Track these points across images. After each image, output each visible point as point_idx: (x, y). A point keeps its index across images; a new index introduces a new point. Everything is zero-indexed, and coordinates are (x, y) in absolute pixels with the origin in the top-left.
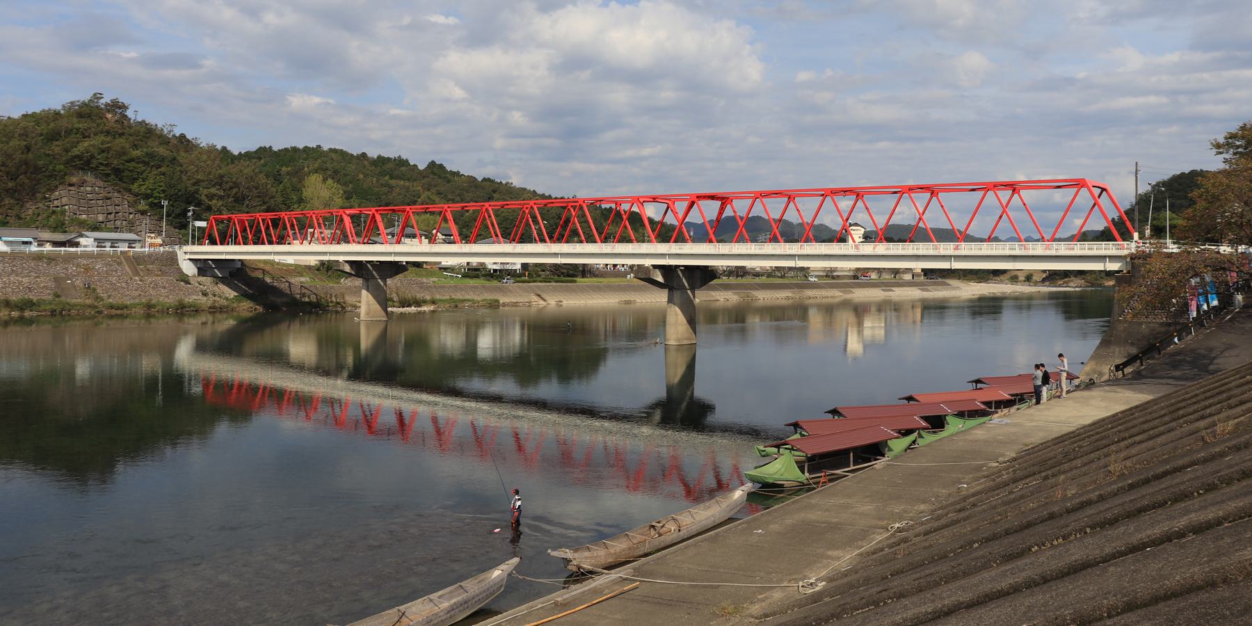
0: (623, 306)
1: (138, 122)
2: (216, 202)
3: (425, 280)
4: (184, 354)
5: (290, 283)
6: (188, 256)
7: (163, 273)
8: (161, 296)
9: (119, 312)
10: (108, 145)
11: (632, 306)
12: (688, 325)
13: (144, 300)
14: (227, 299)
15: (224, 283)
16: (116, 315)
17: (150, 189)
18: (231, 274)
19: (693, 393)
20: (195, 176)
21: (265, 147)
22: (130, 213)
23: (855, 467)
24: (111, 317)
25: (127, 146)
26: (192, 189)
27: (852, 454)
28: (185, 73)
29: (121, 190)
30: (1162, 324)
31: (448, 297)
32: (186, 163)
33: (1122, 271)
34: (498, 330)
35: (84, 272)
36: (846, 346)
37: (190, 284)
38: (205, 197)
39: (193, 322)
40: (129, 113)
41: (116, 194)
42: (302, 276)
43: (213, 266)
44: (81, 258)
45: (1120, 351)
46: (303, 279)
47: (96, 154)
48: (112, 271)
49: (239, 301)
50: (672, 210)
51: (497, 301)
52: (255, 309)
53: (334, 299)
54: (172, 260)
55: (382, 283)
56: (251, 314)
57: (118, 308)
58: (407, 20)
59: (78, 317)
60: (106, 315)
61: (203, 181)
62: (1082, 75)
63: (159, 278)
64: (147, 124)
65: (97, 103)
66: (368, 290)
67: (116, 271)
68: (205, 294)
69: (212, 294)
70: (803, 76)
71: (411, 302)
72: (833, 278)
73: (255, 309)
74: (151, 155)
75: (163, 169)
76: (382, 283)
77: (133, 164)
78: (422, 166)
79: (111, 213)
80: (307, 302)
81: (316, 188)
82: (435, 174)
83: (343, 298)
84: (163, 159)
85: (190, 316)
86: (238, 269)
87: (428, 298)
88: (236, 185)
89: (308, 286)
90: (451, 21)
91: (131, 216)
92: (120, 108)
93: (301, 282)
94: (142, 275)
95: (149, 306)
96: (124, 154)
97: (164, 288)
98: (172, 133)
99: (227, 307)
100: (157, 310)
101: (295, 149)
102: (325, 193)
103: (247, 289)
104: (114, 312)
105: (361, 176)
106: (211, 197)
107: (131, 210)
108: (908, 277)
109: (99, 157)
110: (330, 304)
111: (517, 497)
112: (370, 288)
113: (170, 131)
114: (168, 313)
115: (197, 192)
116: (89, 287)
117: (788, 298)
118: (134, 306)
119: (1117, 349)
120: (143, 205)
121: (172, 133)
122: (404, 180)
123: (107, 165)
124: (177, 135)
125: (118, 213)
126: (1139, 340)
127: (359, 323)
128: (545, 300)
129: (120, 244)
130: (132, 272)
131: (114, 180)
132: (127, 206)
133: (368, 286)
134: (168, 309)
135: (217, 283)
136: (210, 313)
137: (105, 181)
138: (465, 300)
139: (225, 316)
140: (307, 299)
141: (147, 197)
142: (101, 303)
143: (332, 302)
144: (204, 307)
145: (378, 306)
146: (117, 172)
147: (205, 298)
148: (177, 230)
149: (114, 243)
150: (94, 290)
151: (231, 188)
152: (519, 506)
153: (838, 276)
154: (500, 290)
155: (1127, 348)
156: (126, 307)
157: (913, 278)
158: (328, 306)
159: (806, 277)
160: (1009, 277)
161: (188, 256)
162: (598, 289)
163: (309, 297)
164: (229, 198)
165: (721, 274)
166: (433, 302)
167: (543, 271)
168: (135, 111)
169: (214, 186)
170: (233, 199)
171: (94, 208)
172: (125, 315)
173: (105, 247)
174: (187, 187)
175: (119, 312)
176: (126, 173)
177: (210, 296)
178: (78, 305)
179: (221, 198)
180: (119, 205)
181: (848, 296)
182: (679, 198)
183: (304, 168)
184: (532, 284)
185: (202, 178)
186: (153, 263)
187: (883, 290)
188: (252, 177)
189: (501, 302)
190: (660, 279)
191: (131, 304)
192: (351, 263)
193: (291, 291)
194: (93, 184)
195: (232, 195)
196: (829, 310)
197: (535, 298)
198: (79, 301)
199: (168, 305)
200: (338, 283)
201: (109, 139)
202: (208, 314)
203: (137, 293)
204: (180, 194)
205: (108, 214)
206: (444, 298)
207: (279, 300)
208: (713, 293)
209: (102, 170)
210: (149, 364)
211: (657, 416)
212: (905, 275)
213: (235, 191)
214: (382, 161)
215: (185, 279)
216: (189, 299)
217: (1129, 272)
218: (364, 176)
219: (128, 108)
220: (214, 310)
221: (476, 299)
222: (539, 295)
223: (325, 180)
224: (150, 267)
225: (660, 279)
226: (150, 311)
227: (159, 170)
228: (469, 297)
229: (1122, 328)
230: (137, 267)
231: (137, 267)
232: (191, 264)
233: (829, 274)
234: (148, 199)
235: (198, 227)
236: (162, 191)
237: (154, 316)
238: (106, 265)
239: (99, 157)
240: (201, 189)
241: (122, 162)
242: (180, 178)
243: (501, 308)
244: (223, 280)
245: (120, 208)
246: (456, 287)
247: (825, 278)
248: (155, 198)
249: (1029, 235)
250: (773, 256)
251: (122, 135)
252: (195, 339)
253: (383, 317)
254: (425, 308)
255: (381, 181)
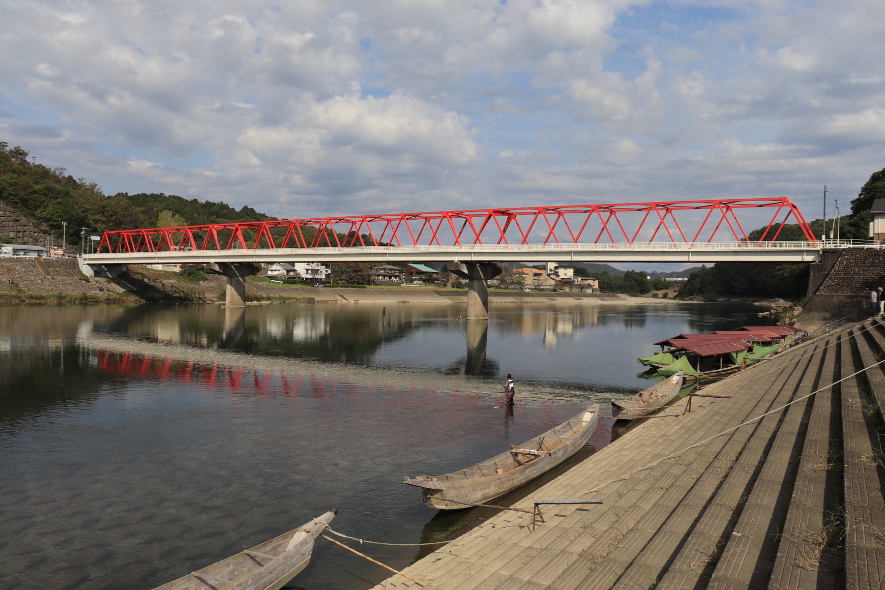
0: (401, 304)
1: (36, 165)
2: (101, 225)
3: (260, 283)
4: (85, 337)
5: (162, 284)
6: (86, 262)
7: (69, 274)
8: (69, 290)
9: (37, 302)
10: (16, 180)
11: (407, 304)
12: (483, 306)
13: (56, 293)
14: (118, 293)
15: (114, 282)
16: (35, 303)
17: (50, 214)
18: (119, 276)
19: (485, 357)
20: (84, 206)
21: (122, 193)
22: (35, 232)
23: (724, 369)
24: (32, 305)
25: (31, 181)
26: (82, 215)
27: (721, 359)
28: (49, 141)
29: (27, 215)
30: (848, 297)
31: (278, 296)
32: (76, 196)
33: (815, 261)
34: (309, 320)
35: (7, 271)
36: (545, 337)
37: (89, 282)
38: (92, 221)
39: (94, 311)
40: (29, 159)
41: (23, 217)
42: (170, 279)
43: (106, 270)
44: (4, 261)
45: (818, 316)
46: (172, 281)
47: (6, 187)
48: (29, 271)
49: (128, 296)
50: (470, 223)
51: (313, 299)
52: (140, 301)
53: (197, 295)
54: (75, 265)
55: (241, 280)
56: (136, 305)
57: (36, 299)
58: (217, 105)
59: (6, 305)
60: (28, 304)
61: (90, 210)
62: (700, 158)
63: (66, 277)
64: (43, 167)
65: (3, 149)
66: (232, 285)
67: (32, 272)
68: (101, 290)
69: (107, 290)
70: (505, 154)
71: (253, 299)
72: (540, 290)
73: (140, 301)
74: (50, 189)
75: (59, 200)
76: (241, 280)
77: (36, 195)
78: (238, 209)
79: (20, 232)
80: (177, 297)
81: (167, 221)
82: (248, 215)
83: (204, 294)
84: (59, 192)
85: (91, 305)
86: (124, 273)
87: (265, 296)
88: (115, 213)
89: (176, 286)
90: (249, 106)
91: (36, 234)
92: (21, 154)
93: (171, 283)
94: (52, 275)
95: (60, 297)
96: (29, 187)
97: (71, 284)
98: (62, 175)
99: (119, 299)
100: (66, 300)
101: (144, 195)
102: (174, 225)
103: (132, 287)
104: (33, 301)
105: (196, 215)
106: (96, 221)
107: (36, 230)
108: (589, 291)
109: (9, 189)
110: (194, 299)
111: (510, 381)
112: (233, 284)
113: (61, 173)
114: (75, 303)
115: (86, 217)
116: (12, 283)
117: (512, 302)
118: (50, 297)
119: (816, 315)
120: (44, 227)
121: (62, 175)
122: (227, 219)
123: (15, 196)
124: (66, 176)
125: (25, 231)
126: (831, 308)
127: (224, 309)
128: (346, 300)
129: (31, 253)
130: (45, 273)
131: (22, 207)
132: (32, 227)
133: (231, 282)
134: (75, 300)
135: (109, 282)
136: (106, 303)
137: (14, 208)
138: (291, 298)
139: (117, 305)
140: (177, 295)
141: (47, 220)
142: (23, 294)
143: (195, 297)
144: (102, 299)
145: (239, 296)
146: (24, 201)
147: (101, 293)
148: (71, 246)
149: (26, 251)
150: (17, 285)
151: (111, 216)
152: (512, 388)
153: (543, 289)
154: (314, 291)
155: (823, 314)
156: (43, 297)
157: (593, 292)
158: (193, 300)
159: (522, 289)
160: (651, 295)
161: (86, 262)
162: (383, 293)
163: (179, 293)
164: (109, 222)
165: (464, 285)
166: (269, 299)
167: (341, 280)
168: (33, 157)
169: (99, 213)
170: (113, 223)
171: (6, 228)
172: (43, 303)
173: (19, 255)
174: (78, 214)
175: (38, 301)
176: (31, 202)
177: (105, 291)
178: (6, 296)
179: (103, 222)
180: (26, 226)
181: (553, 302)
182: (477, 213)
183: (153, 208)
184: (336, 288)
185: (89, 207)
186: (59, 267)
187: (575, 299)
188: (127, 208)
189: (316, 300)
190: (466, 271)
191: (46, 296)
192: (220, 264)
193: (164, 289)
194: (5, 209)
195: (112, 220)
196: (537, 309)
197: (340, 298)
198: (6, 292)
199: (74, 297)
200: (197, 284)
201: (16, 176)
202: (105, 304)
203: (50, 288)
204: (73, 218)
205: (18, 232)
206: (275, 296)
207: (156, 295)
208: (462, 298)
209: (12, 199)
210: (55, 343)
211: (463, 369)
212: (587, 290)
213: (114, 217)
214: (209, 205)
215: (86, 279)
216: (91, 293)
217: (820, 262)
218: (198, 215)
219: (27, 155)
220: (109, 301)
221: (298, 297)
222: (342, 296)
223: (173, 215)
224: (58, 269)
225: (466, 271)
226: (61, 301)
227: (57, 200)
228: (292, 296)
229: (818, 300)
230: (48, 269)
231: (48, 269)
232: (89, 268)
233: (537, 287)
234: (48, 222)
235: (94, 241)
236: (59, 216)
237: (64, 305)
238: (24, 267)
239: (9, 189)
240: (89, 215)
241: (28, 193)
242: (73, 207)
243: (316, 303)
244: (113, 280)
245: (27, 228)
246: (283, 289)
247: (534, 290)
248: (54, 221)
249: (654, 270)
250: (554, 253)
251: (25, 174)
252: (92, 324)
253: (242, 305)
254: (263, 302)
255: (210, 219)
